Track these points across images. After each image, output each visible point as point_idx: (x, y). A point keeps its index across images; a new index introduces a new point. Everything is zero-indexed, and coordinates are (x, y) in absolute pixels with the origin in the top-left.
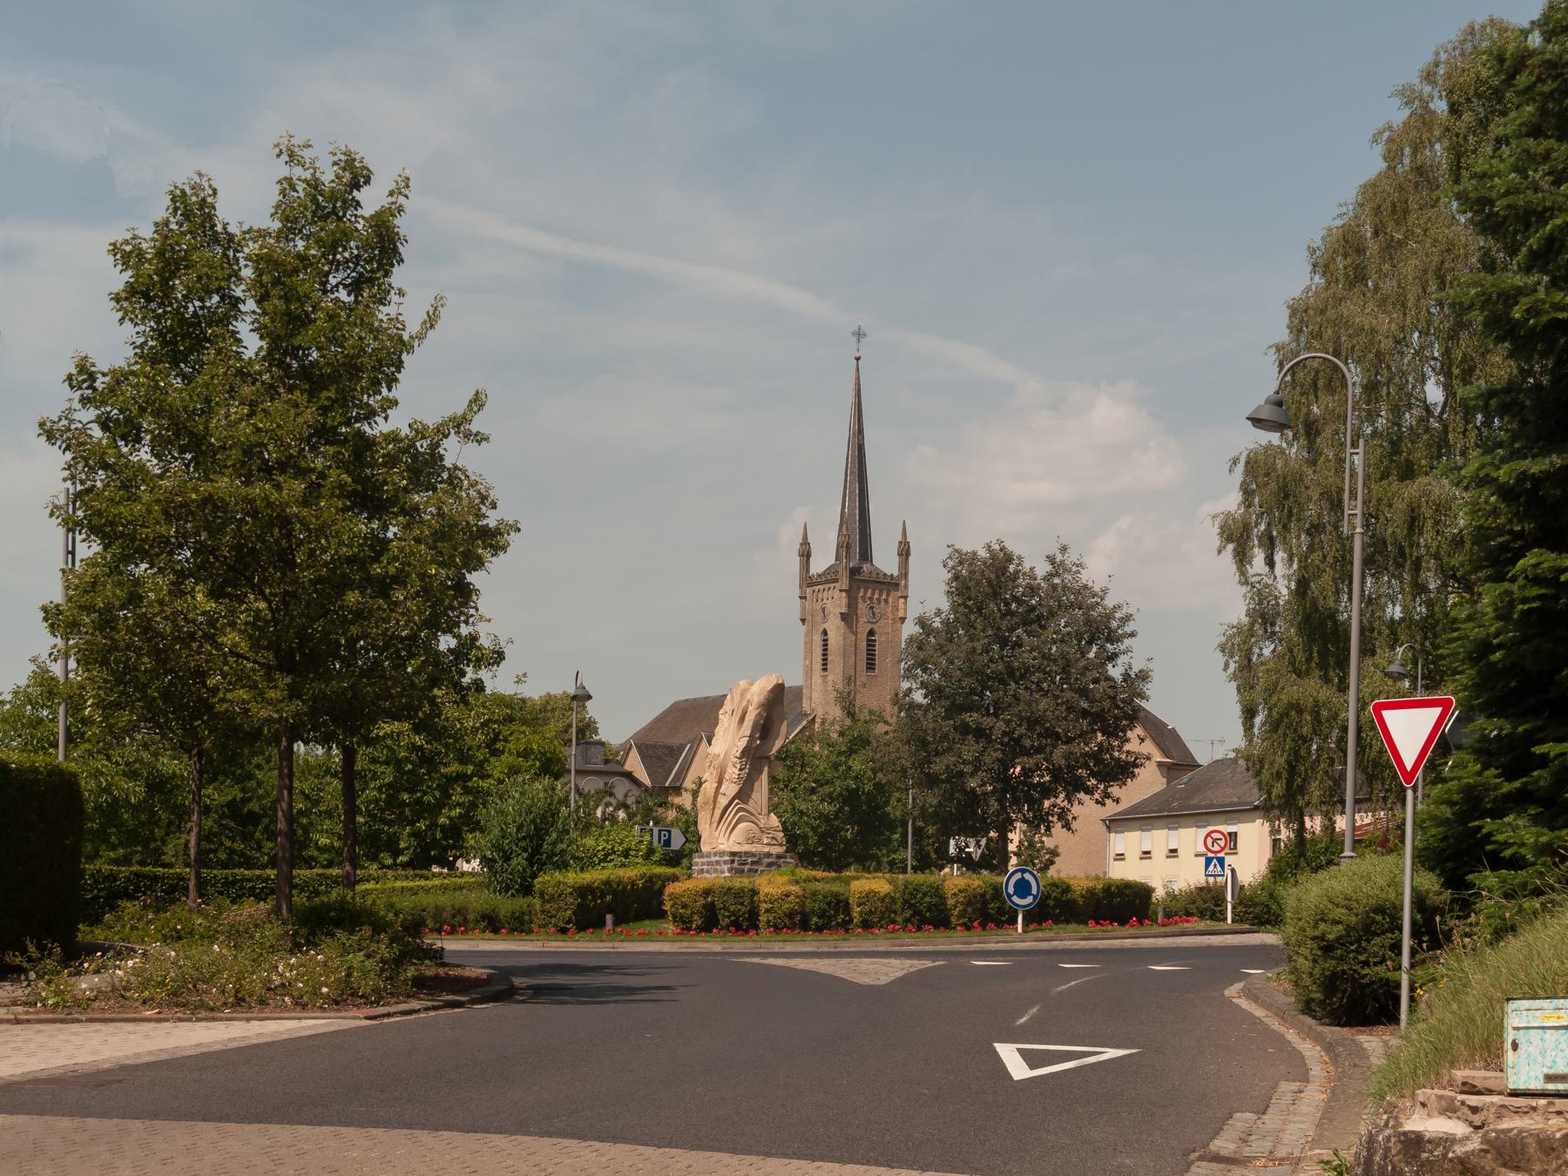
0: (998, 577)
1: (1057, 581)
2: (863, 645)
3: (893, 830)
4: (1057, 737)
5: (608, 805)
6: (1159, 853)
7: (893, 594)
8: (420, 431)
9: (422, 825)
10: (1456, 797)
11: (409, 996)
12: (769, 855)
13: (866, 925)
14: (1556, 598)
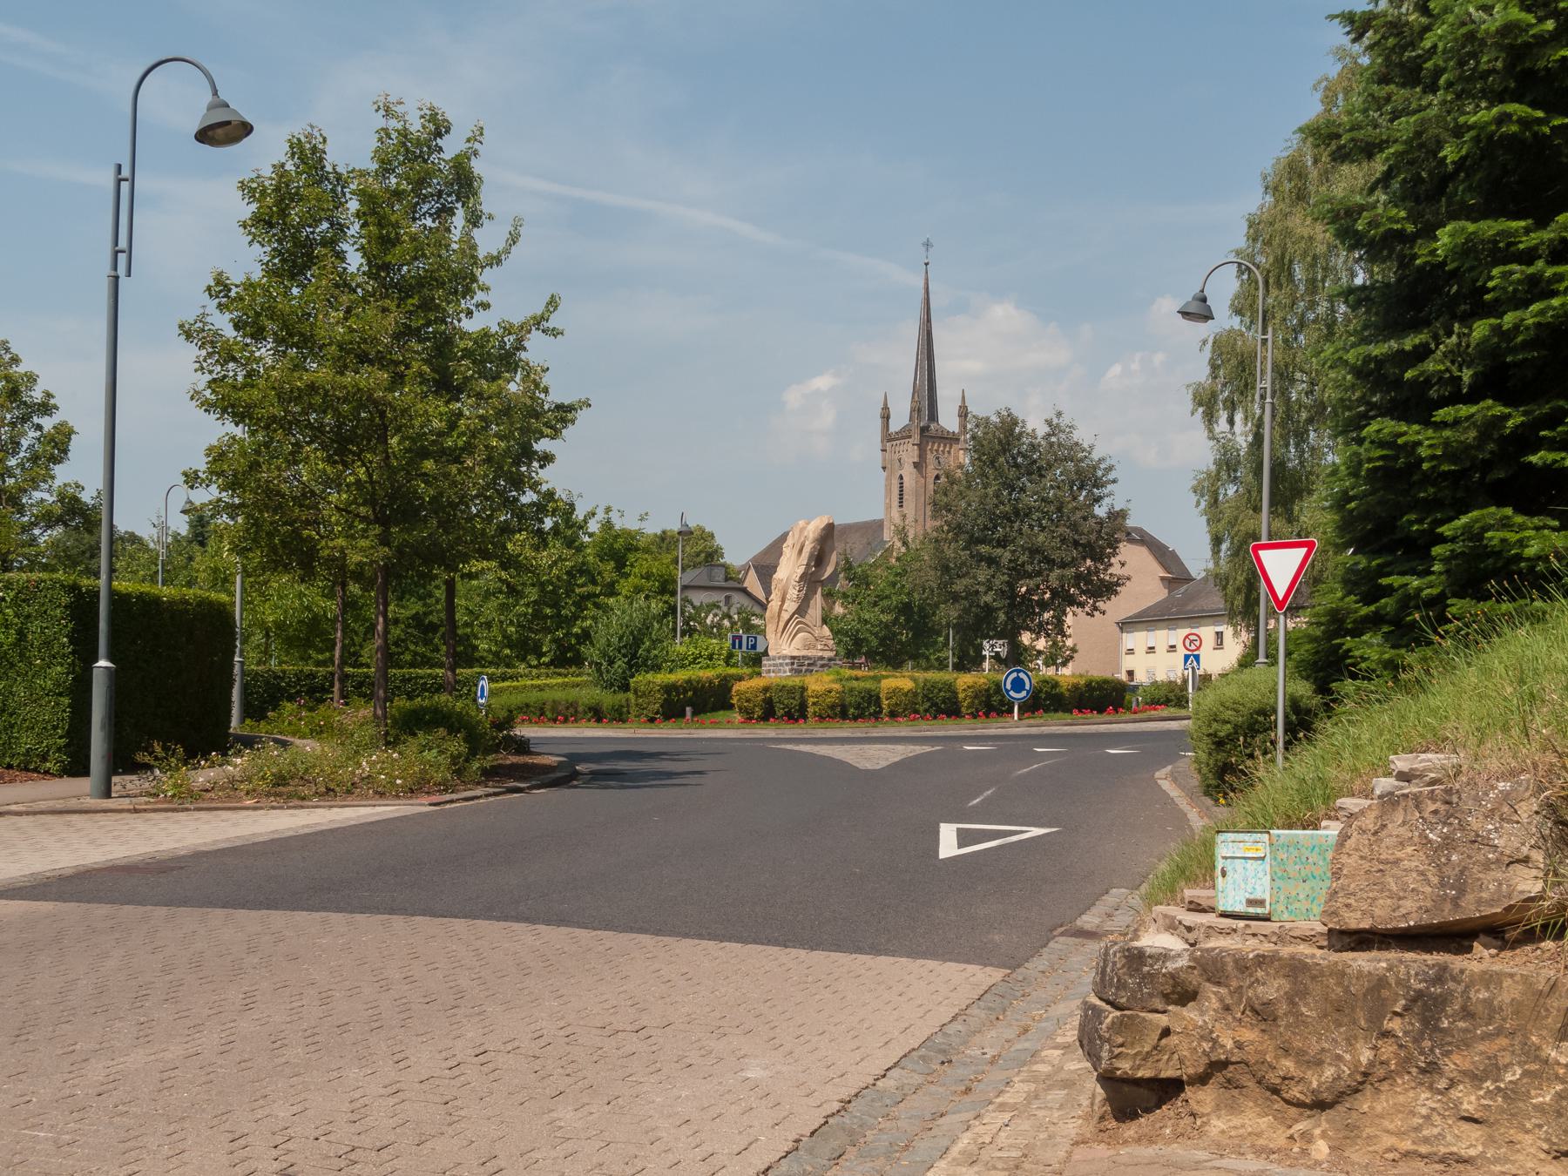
0: (1006, 437)
1: (1053, 439)
3: (939, 634)
4: (1050, 562)
5: (715, 615)
6: (1161, 649)
7: (955, 446)
8: (508, 330)
9: (560, 634)
10: (1323, 619)
11: (478, 783)
12: (822, 658)
13: (893, 715)
14: (1396, 458)
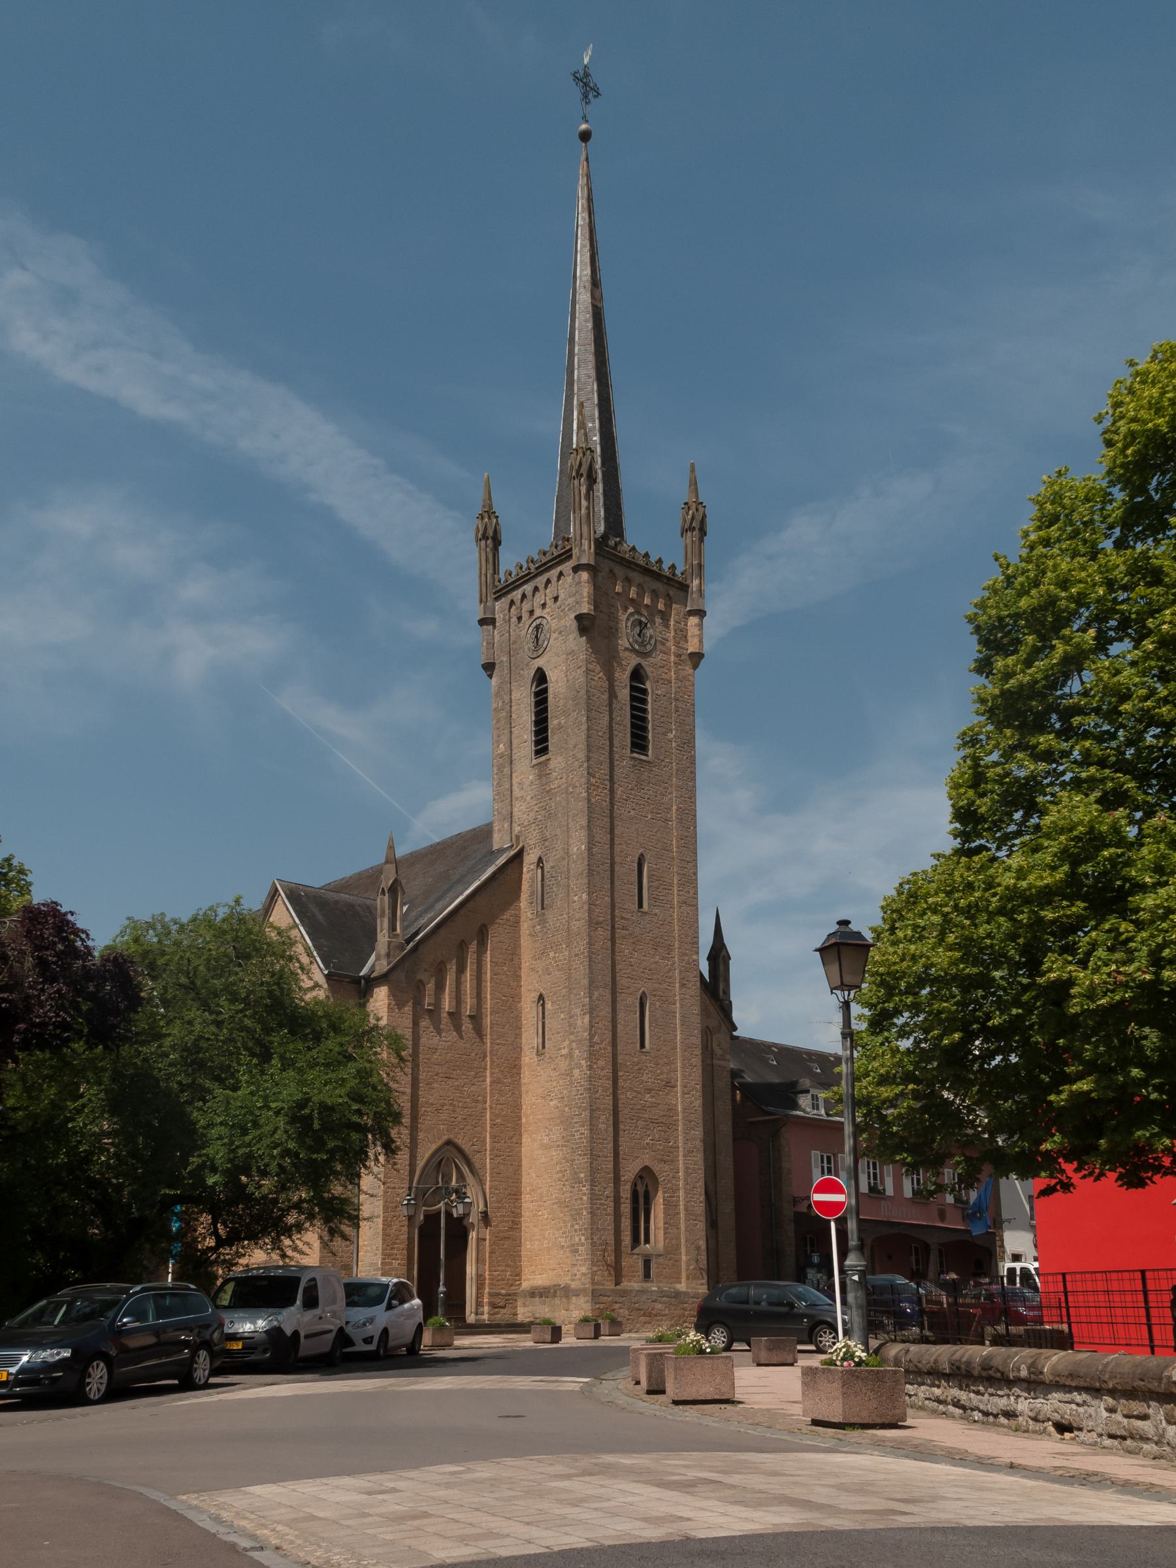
2: (624, 694)
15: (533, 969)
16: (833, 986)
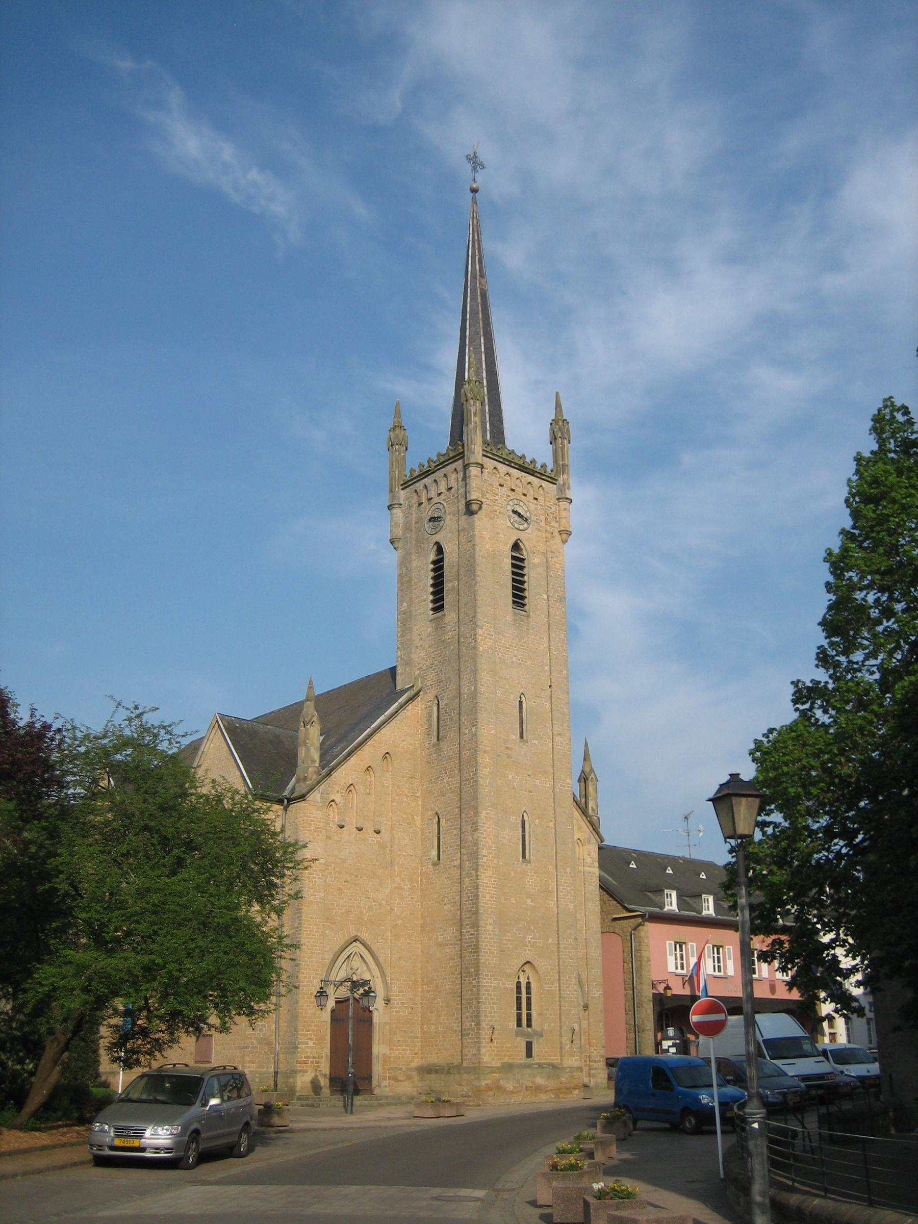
15: (430, 792)
16: (726, 836)
